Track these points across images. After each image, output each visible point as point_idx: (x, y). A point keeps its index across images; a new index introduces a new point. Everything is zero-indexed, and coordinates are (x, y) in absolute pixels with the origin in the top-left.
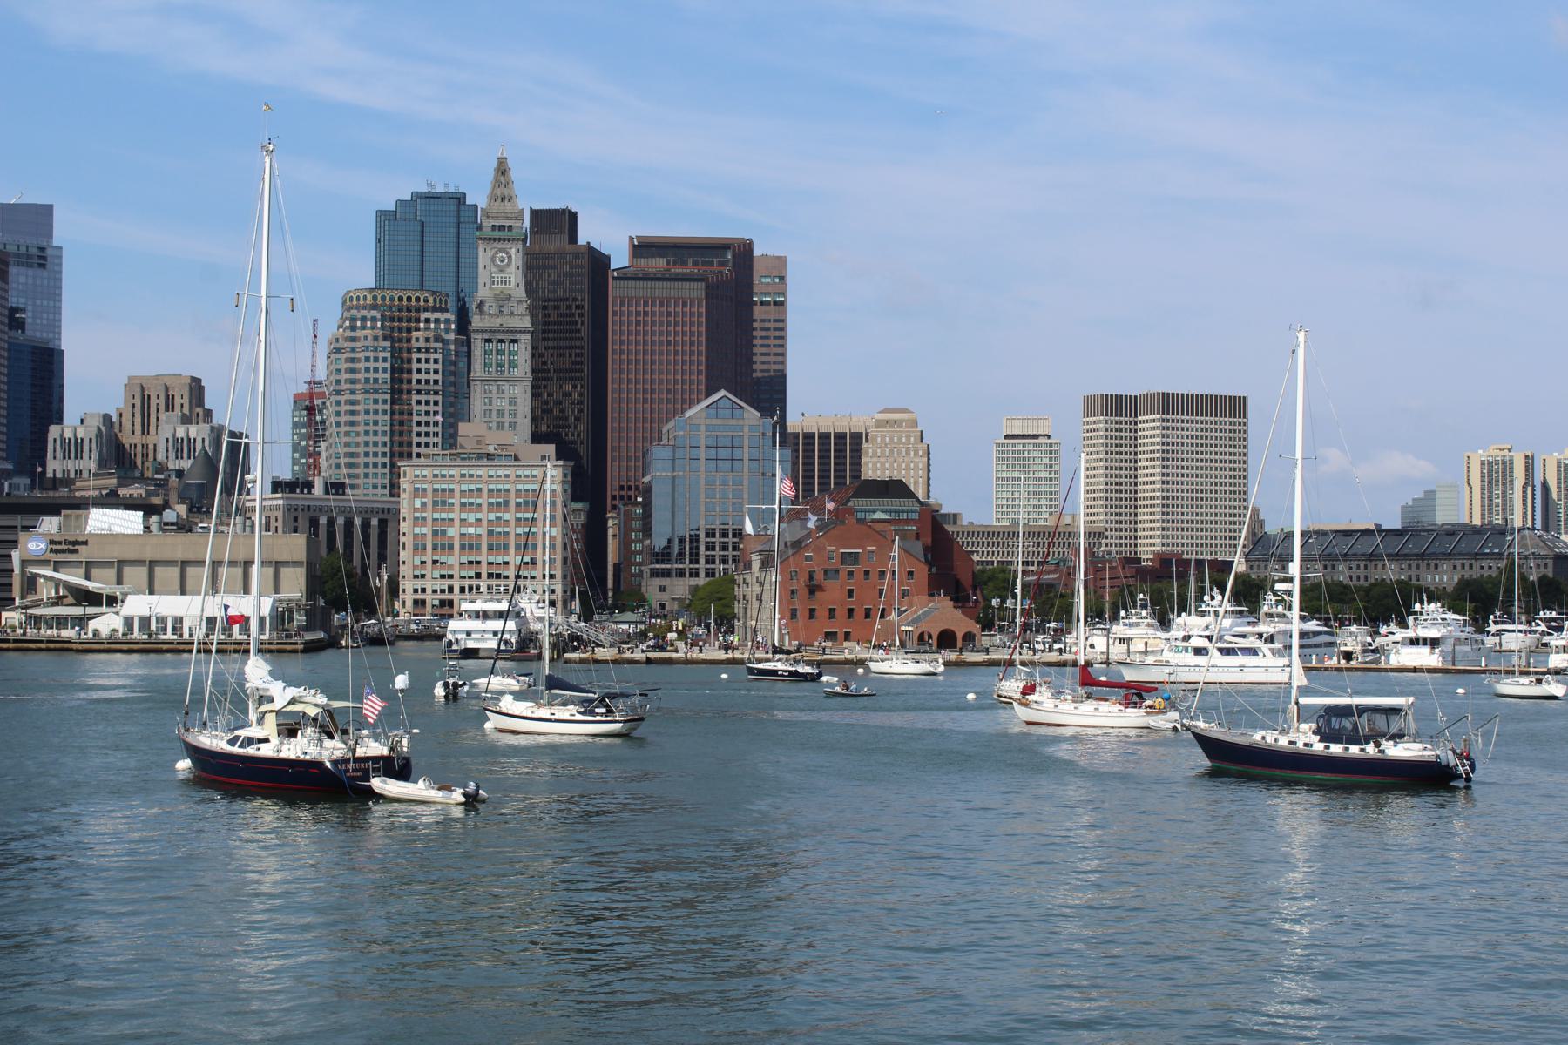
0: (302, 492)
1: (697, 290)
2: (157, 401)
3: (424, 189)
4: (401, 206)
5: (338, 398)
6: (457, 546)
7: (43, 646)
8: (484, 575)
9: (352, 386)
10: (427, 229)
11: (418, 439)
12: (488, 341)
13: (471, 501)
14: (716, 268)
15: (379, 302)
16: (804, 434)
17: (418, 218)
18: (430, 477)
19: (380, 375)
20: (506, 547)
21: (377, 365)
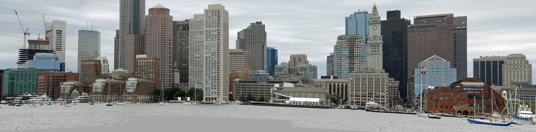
0: (328, 79)
2: (297, 59)
15: (346, 38)
16: (499, 61)
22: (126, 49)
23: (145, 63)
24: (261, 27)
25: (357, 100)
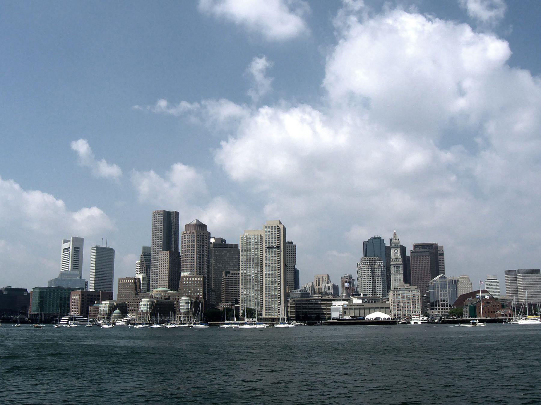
3: (373, 237)
23: (191, 281)
24: (293, 247)
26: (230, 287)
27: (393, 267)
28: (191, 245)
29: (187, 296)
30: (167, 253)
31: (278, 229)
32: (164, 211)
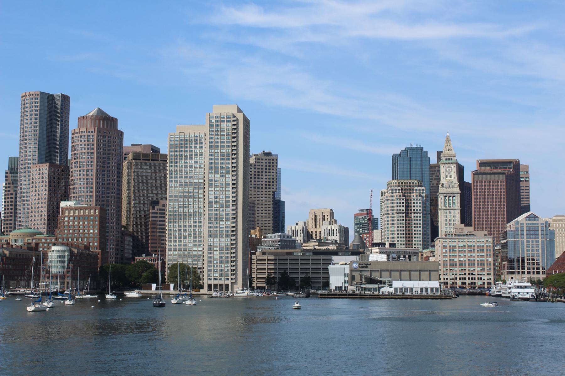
0: (382, 247)
1: (503, 177)
2: (320, 217)
3: (410, 147)
4: (403, 152)
5: (388, 216)
6: (458, 265)
7: (368, 297)
8: (467, 274)
9: (392, 212)
10: (411, 160)
11: (414, 229)
12: (446, 196)
13: (462, 249)
14: (507, 169)
17: (409, 156)
18: (448, 242)
19: (402, 208)
20: (474, 264)
21: (400, 205)
22: (32, 187)
24: (271, 161)
25: (471, 281)
26: (159, 229)
27: (443, 198)
28: (88, 153)
29: (63, 244)
30: (45, 167)
31: (233, 121)
32: (41, 93)
